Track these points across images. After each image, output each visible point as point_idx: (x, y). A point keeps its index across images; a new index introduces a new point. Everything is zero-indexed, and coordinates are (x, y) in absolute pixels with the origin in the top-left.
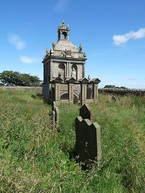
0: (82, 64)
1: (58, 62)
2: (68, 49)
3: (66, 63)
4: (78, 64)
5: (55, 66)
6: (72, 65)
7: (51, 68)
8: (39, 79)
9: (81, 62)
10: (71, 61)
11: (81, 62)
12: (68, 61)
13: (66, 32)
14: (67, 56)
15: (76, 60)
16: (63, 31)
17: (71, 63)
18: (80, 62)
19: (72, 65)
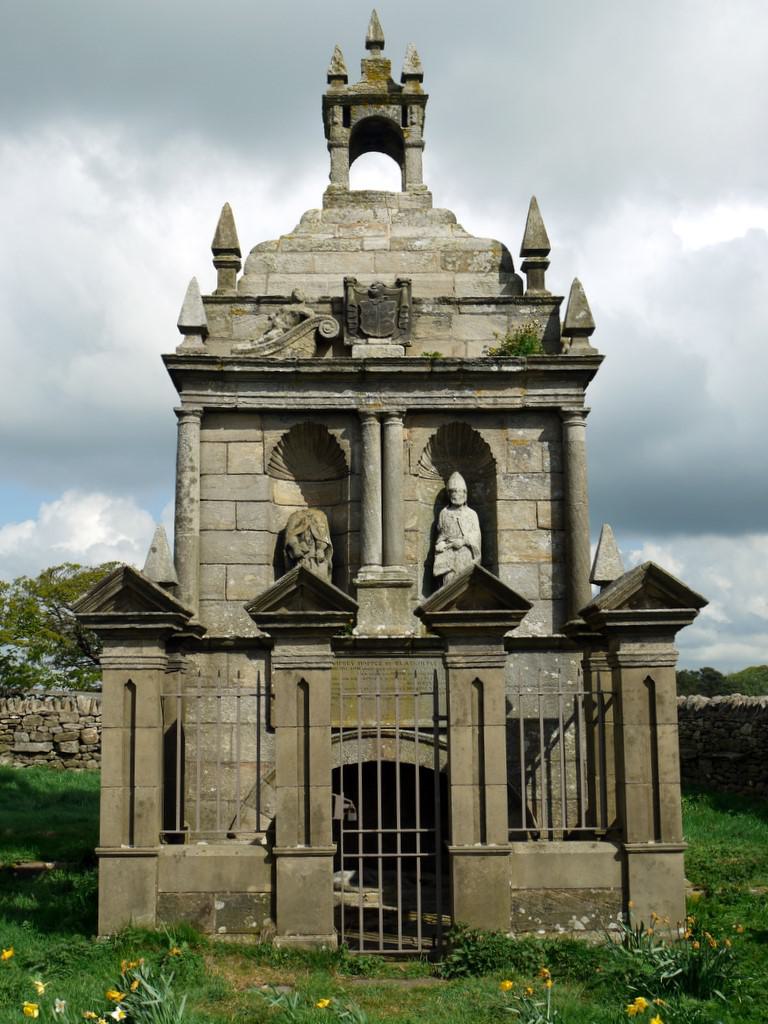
1: (264, 417)
2: (366, 280)
3: (355, 419)
4: (503, 418)
6: (424, 434)
7: (498, 517)
8: (580, 700)
12: (372, 401)
13: (393, 112)
14: (361, 350)
15: (462, 375)
16: (361, 113)
17: (413, 417)
18: (513, 397)
19: (424, 434)
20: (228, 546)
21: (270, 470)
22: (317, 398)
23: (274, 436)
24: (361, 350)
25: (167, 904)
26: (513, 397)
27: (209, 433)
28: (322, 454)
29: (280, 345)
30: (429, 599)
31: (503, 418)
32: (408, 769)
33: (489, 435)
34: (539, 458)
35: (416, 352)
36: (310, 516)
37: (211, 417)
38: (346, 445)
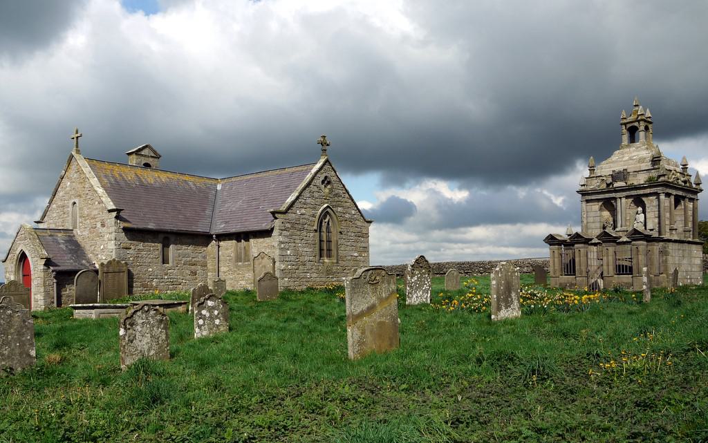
0: (692, 200)
1: (598, 200)
3: (615, 199)
4: (647, 195)
5: (593, 210)
9: (652, 190)
10: (625, 194)
11: (652, 190)
12: (618, 195)
14: (616, 185)
16: (629, 126)
17: (627, 197)
18: (648, 191)
19: (630, 200)
20: (593, 225)
21: (601, 210)
22: (607, 196)
23: (600, 203)
24: (616, 185)
25: (561, 284)
26: (648, 191)
27: (588, 204)
28: (609, 205)
29: (599, 186)
30: (75, 284)
31: (647, 195)
32: (626, 266)
33: (644, 199)
34: (655, 203)
35: (629, 183)
36: (329, 272)
37: (588, 201)
38: (615, 204)
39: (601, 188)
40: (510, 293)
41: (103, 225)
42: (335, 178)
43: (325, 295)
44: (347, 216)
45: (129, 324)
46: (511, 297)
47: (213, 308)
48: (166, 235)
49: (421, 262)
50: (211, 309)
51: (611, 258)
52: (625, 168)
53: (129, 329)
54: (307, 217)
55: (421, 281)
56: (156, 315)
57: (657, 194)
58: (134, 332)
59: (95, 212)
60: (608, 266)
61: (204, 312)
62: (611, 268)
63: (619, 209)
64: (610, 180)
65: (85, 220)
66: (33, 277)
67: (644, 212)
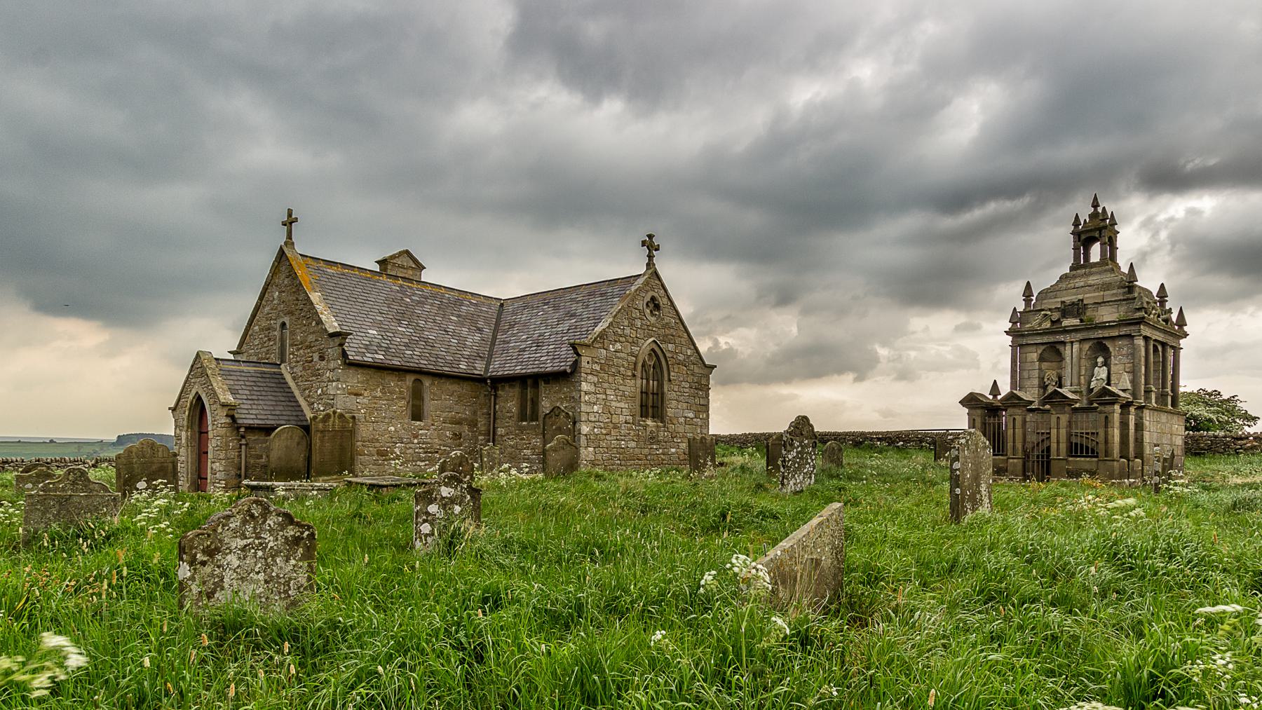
3: (1064, 343)
10: (1079, 336)
12: (1068, 338)
14: (1066, 323)
19: (1086, 346)
22: (1051, 339)
36: (653, 439)
39: (1043, 326)
40: (978, 485)
41: (322, 358)
42: (665, 300)
43: (827, 561)
44: (681, 357)
45: (204, 552)
46: (980, 492)
47: (452, 501)
48: (418, 377)
49: (802, 425)
50: (446, 504)
51: (1063, 432)
52: (1080, 297)
53: (203, 563)
54: (622, 355)
55: (802, 458)
56: (282, 527)
57: (1130, 337)
58: (217, 571)
59: (311, 338)
60: (1058, 442)
61: (433, 508)
62: (1063, 446)
63: (1068, 359)
64: (1056, 316)
65: (298, 350)
66: (210, 435)
67: (1106, 364)
